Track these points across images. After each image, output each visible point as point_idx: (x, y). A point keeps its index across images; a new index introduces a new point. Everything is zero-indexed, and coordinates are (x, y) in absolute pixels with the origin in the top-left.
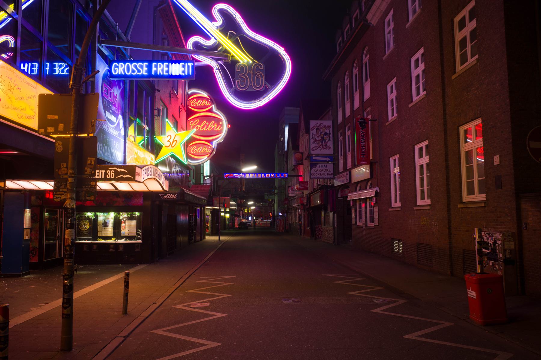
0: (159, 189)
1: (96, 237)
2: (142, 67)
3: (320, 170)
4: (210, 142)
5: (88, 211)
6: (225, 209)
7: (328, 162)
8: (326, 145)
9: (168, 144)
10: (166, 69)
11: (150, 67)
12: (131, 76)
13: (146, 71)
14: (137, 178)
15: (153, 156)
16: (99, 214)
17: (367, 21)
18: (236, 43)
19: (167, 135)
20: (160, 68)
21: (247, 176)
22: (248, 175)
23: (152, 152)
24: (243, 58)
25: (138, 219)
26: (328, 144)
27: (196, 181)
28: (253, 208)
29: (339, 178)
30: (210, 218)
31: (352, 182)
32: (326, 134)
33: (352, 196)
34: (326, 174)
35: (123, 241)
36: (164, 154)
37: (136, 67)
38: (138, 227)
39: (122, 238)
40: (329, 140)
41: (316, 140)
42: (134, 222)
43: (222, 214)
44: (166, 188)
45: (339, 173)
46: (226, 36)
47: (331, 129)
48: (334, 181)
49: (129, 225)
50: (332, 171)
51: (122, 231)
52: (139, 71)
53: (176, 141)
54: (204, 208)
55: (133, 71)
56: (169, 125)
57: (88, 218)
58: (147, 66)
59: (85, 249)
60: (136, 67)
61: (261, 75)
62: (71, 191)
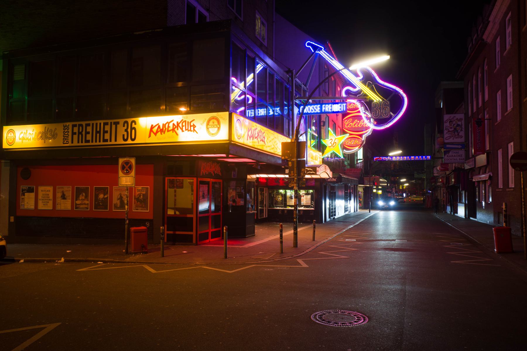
0: (327, 177)
1: (286, 205)
2: (317, 108)
3: (452, 156)
4: (361, 136)
6: (377, 187)
7: (461, 148)
8: (458, 135)
9: (330, 145)
10: (330, 108)
11: (321, 108)
12: (311, 113)
13: (319, 110)
15: (321, 154)
16: (288, 191)
17: (483, 40)
18: (372, 89)
19: (329, 139)
20: (327, 108)
21: (394, 159)
23: (320, 151)
24: (376, 98)
25: (312, 194)
26: (460, 134)
28: (407, 184)
29: (468, 162)
30: (362, 194)
31: (477, 167)
32: (458, 125)
33: (475, 179)
35: (302, 208)
36: (328, 153)
38: (312, 199)
39: (302, 206)
40: (461, 130)
41: (449, 131)
42: (309, 196)
43: (375, 191)
44: (331, 176)
45: (470, 158)
47: (463, 121)
48: (465, 165)
49: (306, 199)
50: (463, 157)
51: (302, 202)
52: (315, 110)
55: (312, 111)
57: (281, 194)
59: (280, 212)
60: (313, 108)
62: (296, 183)
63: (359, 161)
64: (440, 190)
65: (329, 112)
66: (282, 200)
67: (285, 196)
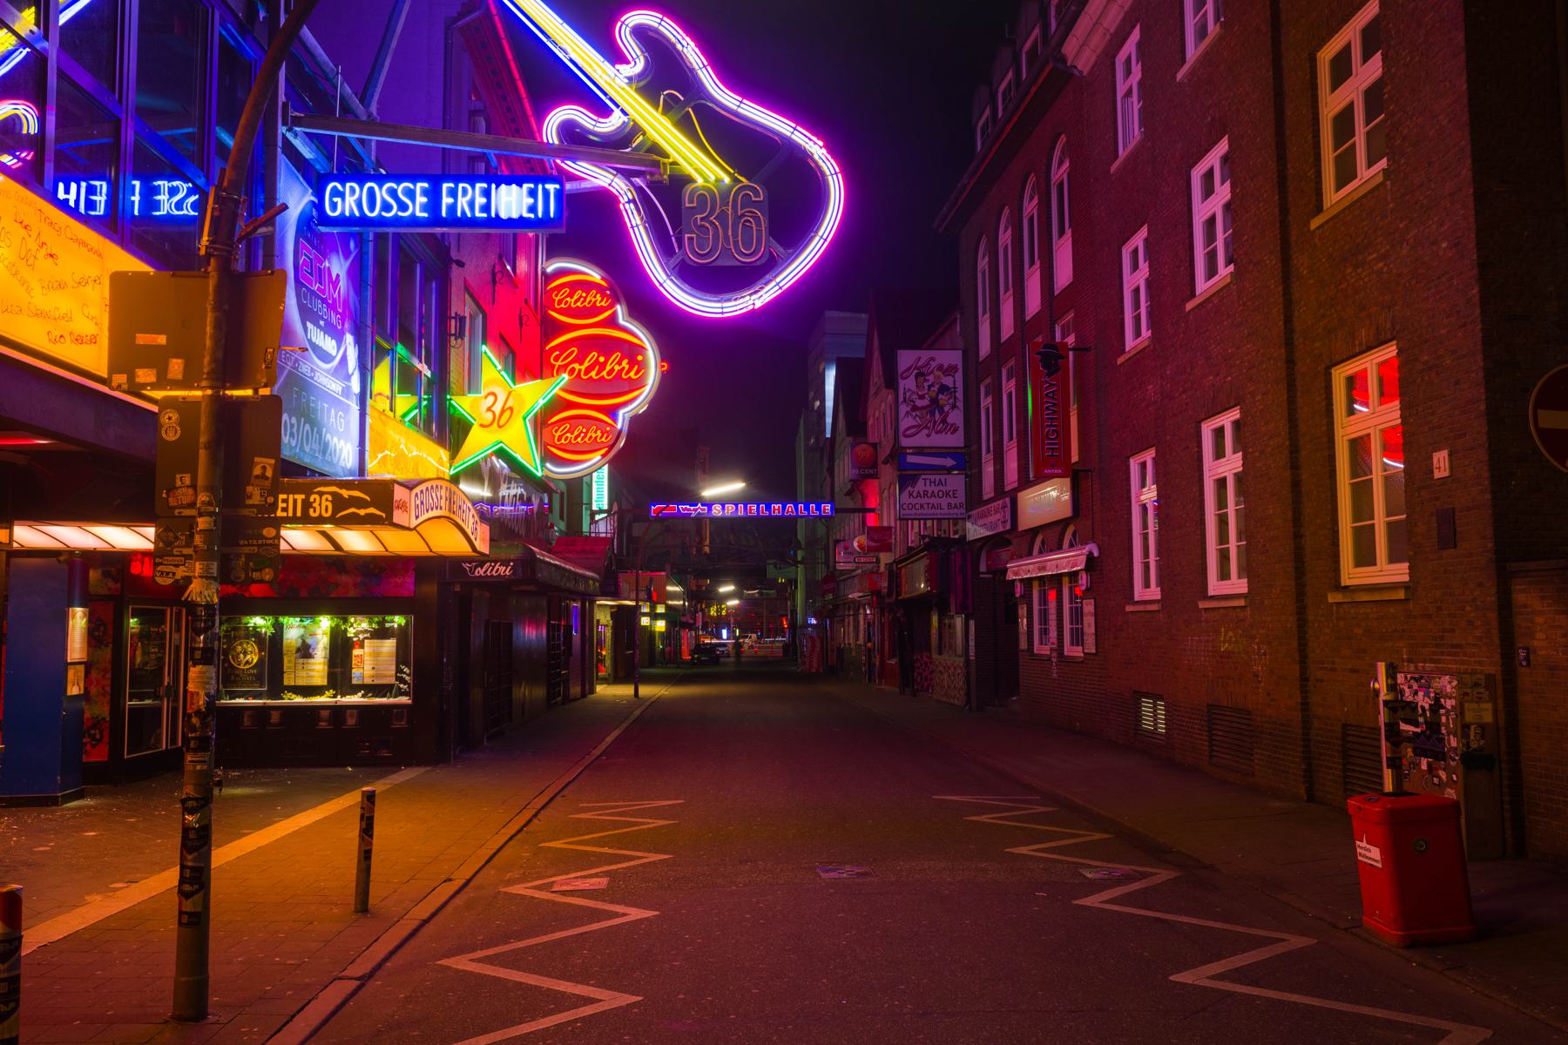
1: (277, 689)
2: (411, 194)
4: (612, 411)
5: (255, 613)
8: (944, 421)
11: (434, 196)
12: (380, 222)
13: (424, 208)
14: (398, 517)
15: (444, 454)
16: (287, 621)
17: (1064, 60)
18: (684, 125)
20: (465, 199)
21: (717, 511)
22: (719, 507)
23: (441, 440)
24: (703, 168)
25: (401, 635)
26: (949, 420)
27: (568, 526)
28: (733, 603)
30: (609, 633)
32: (944, 389)
33: (1021, 569)
34: (945, 506)
35: (356, 699)
37: (393, 193)
38: (401, 658)
39: (354, 689)
40: (954, 407)
41: (915, 408)
42: (389, 645)
43: (645, 621)
44: (483, 546)
46: (656, 107)
47: (959, 376)
48: (969, 525)
49: (376, 654)
51: (356, 672)
52: (403, 207)
53: (511, 409)
54: (592, 602)
55: (387, 207)
56: (492, 367)
57: (256, 634)
58: (425, 192)
59: (247, 722)
60: (393, 193)
61: (756, 218)
62: (206, 556)
63: (597, 517)
64: (856, 615)
65: (473, 222)
66: (261, 660)
67: (273, 646)
